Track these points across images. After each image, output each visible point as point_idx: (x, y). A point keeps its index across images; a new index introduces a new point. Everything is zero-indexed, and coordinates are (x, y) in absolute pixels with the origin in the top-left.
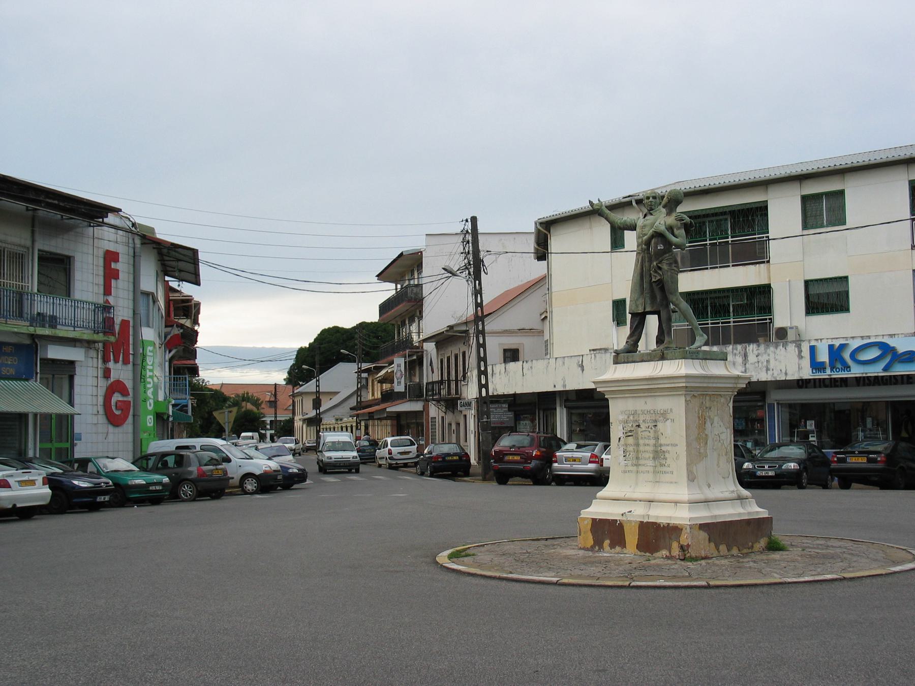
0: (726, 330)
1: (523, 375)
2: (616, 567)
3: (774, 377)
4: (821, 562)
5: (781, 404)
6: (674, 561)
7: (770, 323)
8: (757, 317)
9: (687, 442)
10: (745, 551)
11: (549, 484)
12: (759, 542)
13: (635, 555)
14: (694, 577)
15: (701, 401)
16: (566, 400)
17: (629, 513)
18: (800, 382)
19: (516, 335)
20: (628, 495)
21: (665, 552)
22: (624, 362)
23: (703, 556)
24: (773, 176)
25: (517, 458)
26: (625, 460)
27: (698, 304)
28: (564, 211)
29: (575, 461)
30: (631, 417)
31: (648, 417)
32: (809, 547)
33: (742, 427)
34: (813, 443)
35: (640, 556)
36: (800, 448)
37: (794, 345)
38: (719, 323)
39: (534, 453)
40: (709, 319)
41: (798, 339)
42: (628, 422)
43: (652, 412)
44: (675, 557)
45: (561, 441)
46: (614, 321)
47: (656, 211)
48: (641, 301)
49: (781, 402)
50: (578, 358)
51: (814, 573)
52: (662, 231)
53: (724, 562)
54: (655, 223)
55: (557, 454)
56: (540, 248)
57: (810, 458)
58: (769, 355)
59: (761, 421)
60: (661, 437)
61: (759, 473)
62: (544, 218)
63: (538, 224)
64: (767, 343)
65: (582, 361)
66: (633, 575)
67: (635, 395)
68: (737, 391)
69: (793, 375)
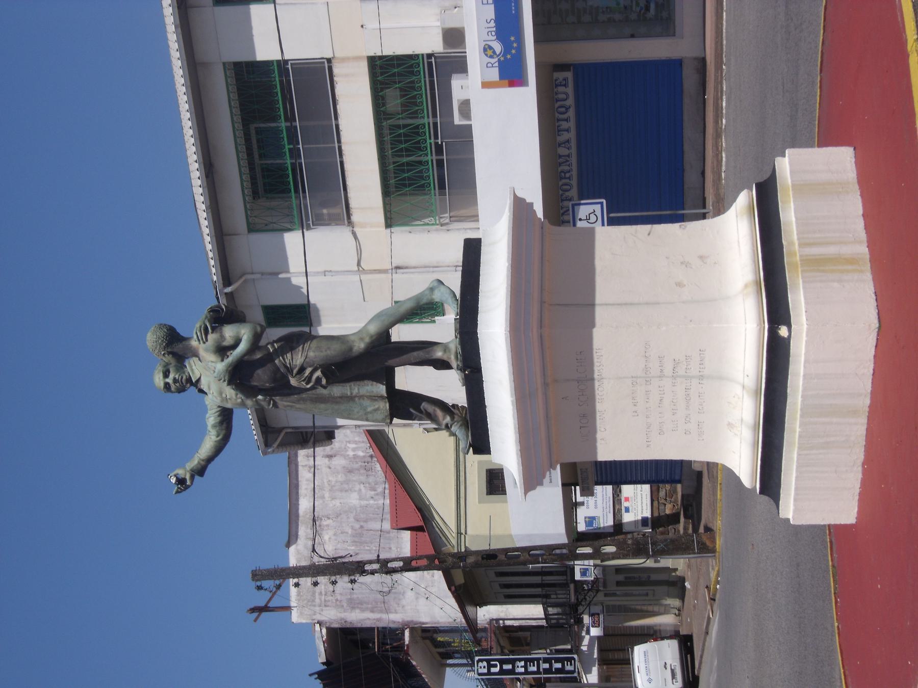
7: (435, 58)
46: (434, 321)
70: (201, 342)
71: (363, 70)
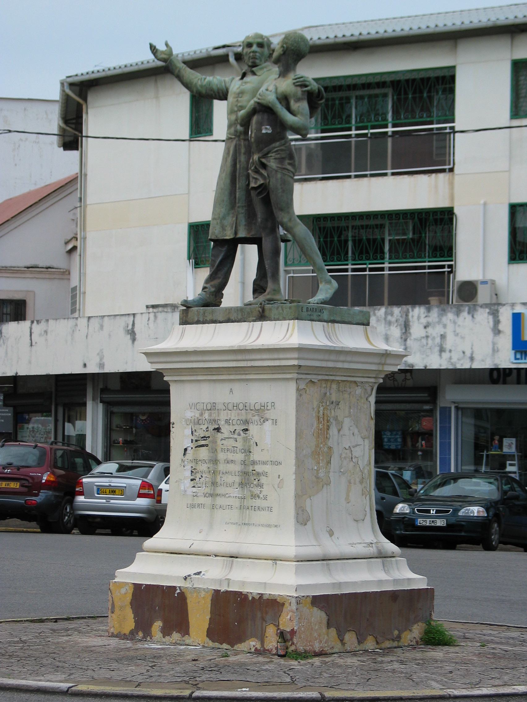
0: (376, 281)
1: (31, 345)
2: (171, 666)
3: (452, 364)
4: (511, 666)
5: (462, 409)
6: (267, 658)
8: (429, 262)
9: (297, 458)
10: (387, 644)
11: (68, 531)
12: (410, 630)
13: (204, 647)
14: (300, 685)
15: (323, 390)
16: (103, 391)
17: (197, 576)
18: (495, 373)
19: (23, 276)
20: (197, 546)
21: (254, 643)
22: (198, 322)
23: (317, 650)
24: (467, 25)
25: (14, 485)
26: (194, 487)
27: (332, 237)
28: (112, 65)
29: (113, 492)
30: (206, 415)
31: (233, 415)
32: (492, 642)
33: (396, 446)
34: (513, 475)
35: (213, 648)
36: (490, 483)
37: (487, 310)
38: (364, 270)
39: (45, 478)
40: (350, 262)
41: (494, 301)
42: (200, 422)
43: (241, 407)
44: (270, 651)
45: (92, 459)
46: (189, 259)
47: (262, 68)
48: (230, 220)
49: (461, 406)
50: (126, 318)
51: (497, 682)
52: (269, 102)
53: (351, 661)
54: (260, 88)
55: (84, 480)
56: (68, 128)
57: (505, 499)
58: (445, 326)
59: (429, 435)
60: (254, 449)
61: (421, 522)
62: (77, 75)
63: (66, 84)
64: (442, 306)
65: (133, 324)
66: (197, 679)
67: (215, 377)
68: (383, 376)
69: (483, 361)
70: (295, 81)
71: (442, 203)
